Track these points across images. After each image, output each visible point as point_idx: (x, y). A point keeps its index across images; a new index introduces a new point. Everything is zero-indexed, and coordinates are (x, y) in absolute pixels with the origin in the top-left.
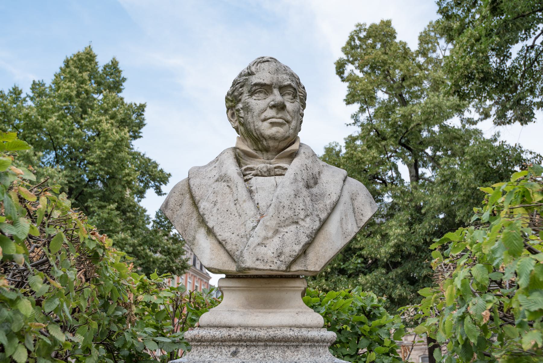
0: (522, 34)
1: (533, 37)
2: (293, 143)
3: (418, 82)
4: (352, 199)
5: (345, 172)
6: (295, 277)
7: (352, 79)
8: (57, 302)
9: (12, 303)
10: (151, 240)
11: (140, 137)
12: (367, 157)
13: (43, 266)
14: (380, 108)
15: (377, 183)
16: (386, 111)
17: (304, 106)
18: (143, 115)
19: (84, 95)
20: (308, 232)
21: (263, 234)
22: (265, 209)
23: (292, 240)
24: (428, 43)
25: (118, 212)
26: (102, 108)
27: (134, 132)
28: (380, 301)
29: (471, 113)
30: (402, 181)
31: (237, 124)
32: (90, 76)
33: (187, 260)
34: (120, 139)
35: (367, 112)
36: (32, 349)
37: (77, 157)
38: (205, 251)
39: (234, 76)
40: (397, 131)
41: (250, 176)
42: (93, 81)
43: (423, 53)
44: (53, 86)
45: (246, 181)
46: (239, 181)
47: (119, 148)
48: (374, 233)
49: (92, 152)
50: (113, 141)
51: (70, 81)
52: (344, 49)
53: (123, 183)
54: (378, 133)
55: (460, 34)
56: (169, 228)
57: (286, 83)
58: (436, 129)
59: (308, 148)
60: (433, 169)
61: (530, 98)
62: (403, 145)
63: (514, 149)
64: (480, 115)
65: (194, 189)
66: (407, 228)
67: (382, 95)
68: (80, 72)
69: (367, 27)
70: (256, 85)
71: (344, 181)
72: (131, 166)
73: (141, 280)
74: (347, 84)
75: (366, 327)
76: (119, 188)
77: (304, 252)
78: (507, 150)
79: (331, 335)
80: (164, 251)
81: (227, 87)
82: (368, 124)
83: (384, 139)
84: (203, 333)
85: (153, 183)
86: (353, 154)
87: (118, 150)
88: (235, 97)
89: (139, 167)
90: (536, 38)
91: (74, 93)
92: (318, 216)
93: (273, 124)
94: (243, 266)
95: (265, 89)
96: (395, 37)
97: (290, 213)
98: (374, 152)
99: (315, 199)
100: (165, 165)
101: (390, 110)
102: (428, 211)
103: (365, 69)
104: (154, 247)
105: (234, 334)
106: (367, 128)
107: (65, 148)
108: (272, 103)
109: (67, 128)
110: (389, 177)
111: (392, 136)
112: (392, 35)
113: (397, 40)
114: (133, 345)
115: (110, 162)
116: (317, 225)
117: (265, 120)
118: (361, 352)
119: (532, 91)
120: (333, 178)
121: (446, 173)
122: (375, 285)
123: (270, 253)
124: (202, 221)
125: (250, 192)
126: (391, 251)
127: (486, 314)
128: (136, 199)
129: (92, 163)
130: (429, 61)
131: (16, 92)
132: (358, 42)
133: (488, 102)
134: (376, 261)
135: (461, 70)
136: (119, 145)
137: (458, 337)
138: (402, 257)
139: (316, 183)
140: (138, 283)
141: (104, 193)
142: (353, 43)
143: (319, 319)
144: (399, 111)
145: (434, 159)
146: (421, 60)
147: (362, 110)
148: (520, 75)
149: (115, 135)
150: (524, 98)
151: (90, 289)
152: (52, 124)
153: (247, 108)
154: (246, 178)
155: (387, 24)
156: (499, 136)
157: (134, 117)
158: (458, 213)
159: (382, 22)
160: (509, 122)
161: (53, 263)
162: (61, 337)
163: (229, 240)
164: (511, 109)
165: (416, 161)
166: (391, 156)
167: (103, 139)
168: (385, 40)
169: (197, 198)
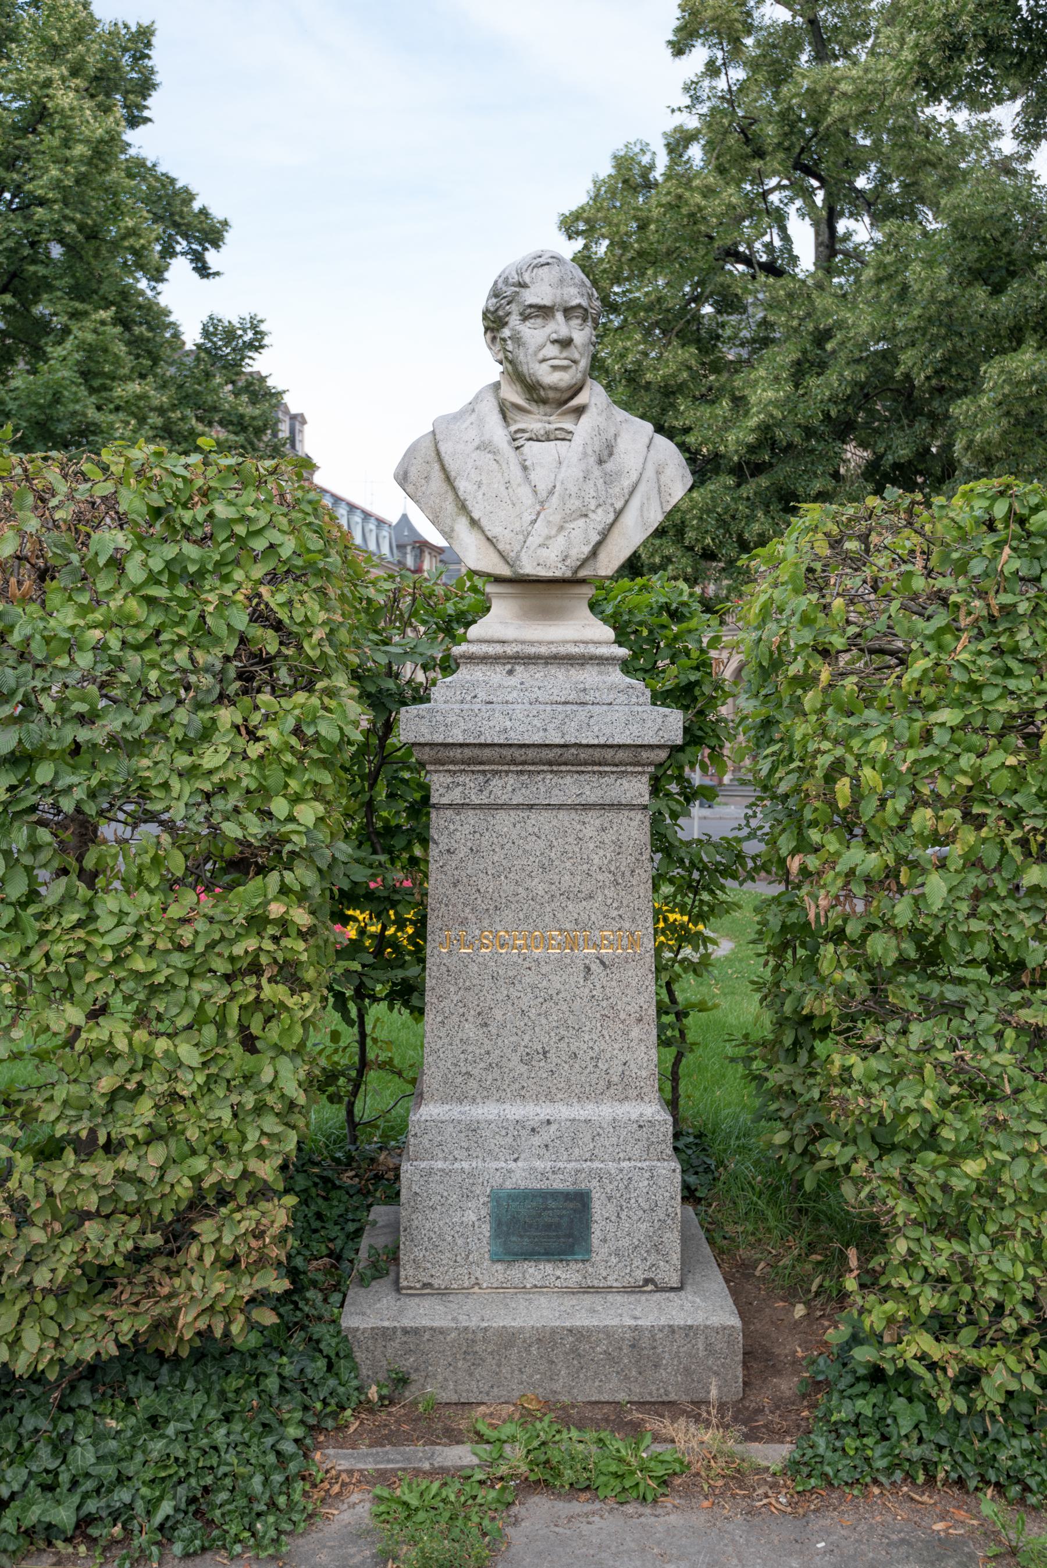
6: (583, 581)
10: (198, 393)
16: (774, 67)
18: (149, 57)
21: (545, 532)
23: (578, 540)
28: (691, 595)
34: (107, 137)
35: (723, 76)
40: (792, 133)
47: (104, 161)
50: (87, 141)
66: (789, 388)
70: (531, 306)
77: (594, 553)
79: (623, 652)
80: (231, 423)
84: (473, 649)
85: (184, 243)
86: (680, 197)
87: (103, 166)
88: (500, 318)
93: (555, 368)
97: (578, 503)
99: (609, 479)
105: (510, 650)
108: (554, 336)
111: (780, 144)
116: (611, 517)
117: (544, 360)
118: (660, 664)
122: (709, 512)
124: (463, 507)
125: (525, 468)
126: (751, 439)
135: (937, 29)
136: (106, 149)
139: (611, 454)
149: (92, 125)
153: (517, 339)
157: (126, 60)
158: (902, 357)
167: (60, 133)
169: (453, 474)
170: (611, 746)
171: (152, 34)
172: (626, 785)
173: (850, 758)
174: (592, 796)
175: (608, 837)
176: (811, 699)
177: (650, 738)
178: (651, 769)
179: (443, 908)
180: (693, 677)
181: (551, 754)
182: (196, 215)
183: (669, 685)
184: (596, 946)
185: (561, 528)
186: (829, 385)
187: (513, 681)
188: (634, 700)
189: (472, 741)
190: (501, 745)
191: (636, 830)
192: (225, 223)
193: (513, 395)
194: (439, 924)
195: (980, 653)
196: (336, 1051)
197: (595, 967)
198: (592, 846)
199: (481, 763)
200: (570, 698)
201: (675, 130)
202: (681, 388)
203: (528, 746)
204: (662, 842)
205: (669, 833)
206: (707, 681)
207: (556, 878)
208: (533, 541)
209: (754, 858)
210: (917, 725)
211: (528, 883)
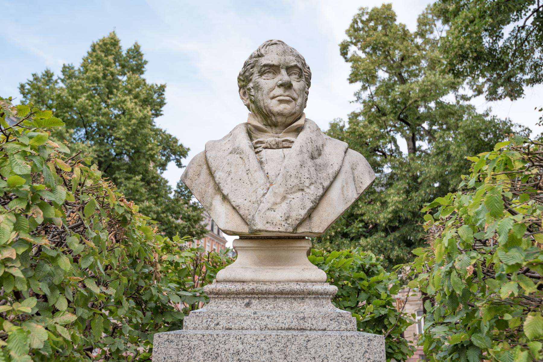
0: (513, 15)
1: (524, 18)
2: (299, 118)
3: (416, 62)
4: (353, 169)
6: (302, 238)
7: (355, 60)
8: (92, 259)
9: (53, 260)
10: (173, 207)
11: (161, 115)
12: (368, 132)
13: (79, 228)
14: (381, 86)
15: (377, 155)
16: (386, 89)
17: (309, 85)
18: (163, 94)
19: (110, 77)
20: (312, 198)
21: (272, 200)
22: (274, 178)
23: (298, 205)
25: (143, 183)
26: (126, 89)
27: (156, 110)
28: (378, 260)
29: (465, 90)
30: (400, 153)
31: (248, 101)
32: (115, 59)
35: (368, 89)
36: (71, 299)
37: (105, 133)
38: (221, 216)
39: (245, 58)
41: (260, 149)
42: (117, 64)
43: (421, 34)
45: (257, 153)
46: (251, 153)
47: (143, 125)
50: (137, 119)
51: (97, 64)
52: (348, 32)
53: (147, 157)
54: (379, 110)
55: (455, 16)
56: (189, 197)
57: (293, 64)
58: (432, 105)
59: (313, 123)
60: (430, 142)
61: (520, 76)
62: (399, 119)
63: (505, 123)
64: (474, 91)
65: (210, 160)
66: (404, 196)
67: (382, 74)
68: (106, 56)
69: (369, 10)
70: (265, 66)
71: (345, 152)
74: (350, 64)
75: (365, 283)
77: (309, 216)
78: (499, 124)
79: (333, 288)
81: (239, 69)
82: (370, 101)
83: (384, 115)
84: (220, 287)
86: (355, 129)
87: (141, 126)
88: (247, 77)
89: (161, 142)
90: (527, 19)
91: (100, 75)
92: (321, 183)
93: (281, 101)
95: (274, 69)
96: (395, 20)
97: (296, 181)
98: (374, 127)
99: (319, 169)
100: (184, 141)
101: (390, 88)
102: (424, 180)
104: (176, 214)
105: (247, 287)
107: (94, 125)
108: (280, 82)
109: (96, 107)
110: (389, 150)
112: (392, 18)
113: (397, 23)
114: (159, 298)
115: (135, 138)
116: (321, 191)
117: (273, 98)
119: (522, 69)
120: (335, 150)
121: (440, 145)
122: (375, 247)
123: (278, 217)
124: (218, 189)
125: (261, 163)
126: (390, 216)
128: (159, 171)
129: (119, 139)
130: (427, 42)
131: (48, 75)
132: (360, 25)
133: (481, 80)
134: (376, 226)
135: (456, 50)
136: (143, 122)
137: (446, 289)
138: (400, 222)
139: (320, 155)
140: (162, 245)
141: (130, 166)
142: (356, 26)
143: (322, 275)
144: (399, 89)
145: (430, 133)
146: (419, 41)
147: (364, 88)
150: (514, 75)
151: (120, 249)
152: (82, 103)
153: (257, 87)
154: (256, 150)
155: (388, 7)
156: (491, 111)
157: (155, 96)
158: (451, 182)
159: (384, 5)
161: (87, 226)
162: (97, 290)
163: (242, 206)
164: (502, 86)
166: (390, 131)
168: (386, 22)
169: (213, 169)
171: (165, 87)
180: (383, 312)
182: (178, 147)
183: (368, 317)
185: (284, 198)
186: (421, 195)
187: (248, 311)
188: (343, 326)
192: (189, 149)
200: (293, 325)
201: (352, 113)
206: (392, 315)
208: (264, 206)
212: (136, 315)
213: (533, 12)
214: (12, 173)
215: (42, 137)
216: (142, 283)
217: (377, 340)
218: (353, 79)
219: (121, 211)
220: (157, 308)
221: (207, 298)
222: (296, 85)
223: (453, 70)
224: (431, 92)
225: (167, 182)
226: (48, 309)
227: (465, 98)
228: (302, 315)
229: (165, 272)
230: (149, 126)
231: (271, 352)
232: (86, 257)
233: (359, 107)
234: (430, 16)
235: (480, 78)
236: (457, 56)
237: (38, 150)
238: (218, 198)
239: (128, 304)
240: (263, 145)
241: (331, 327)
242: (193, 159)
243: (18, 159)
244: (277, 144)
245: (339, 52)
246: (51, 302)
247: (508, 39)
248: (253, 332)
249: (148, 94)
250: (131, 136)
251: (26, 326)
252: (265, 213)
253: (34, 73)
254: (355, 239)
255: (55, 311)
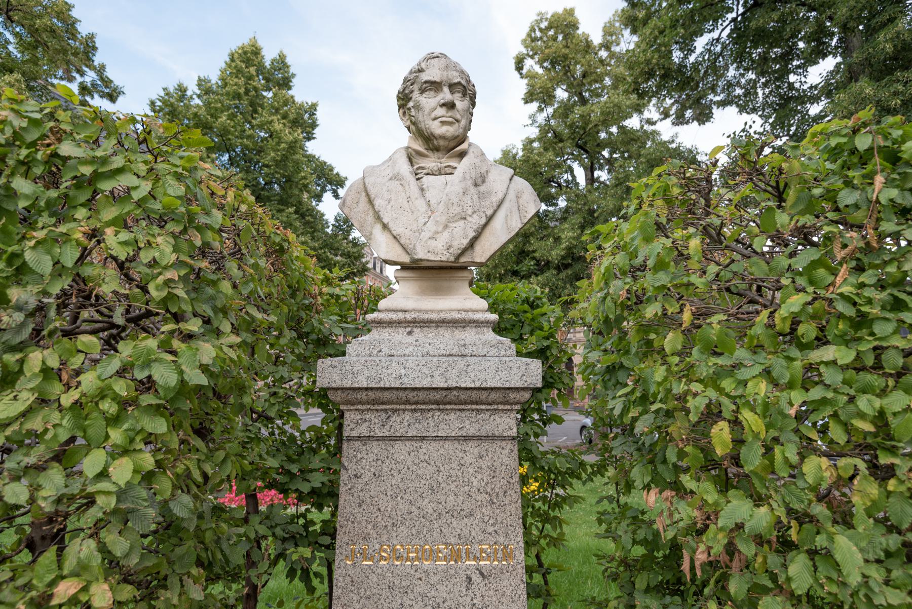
0: (708, 26)
1: (720, 28)
2: (463, 142)
3: (599, 79)
4: (518, 197)
5: (512, 171)
6: (464, 268)
7: (531, 76)
8: (252, 285)
9: (214, 283)
11: (314, 138)
12: (543, 160)
13: (237, 253)
14: (559, 107)
15: (552, 187)
16: (565, 110)
17: (473, 104)
19: (253, 93)
20: (475, 227)
21: (434, 229)
22: (435, 206)
23: (460, 235)
24: (612, 35)
25: (297, 216)
26: (273, 107)
27: (308, 133)
28: (542, 293)
29: (651, 112)
30: (577, 184)
31: (408, 123)
32: (257, 71)
33: (367, 263)
36: (234, 322)
37: (252, 159)
38: (381, 247)
39: (404, 73)
41: (421, 175)
42: (261, 77)
43: (606, 46)
44: (220, 83)
45: (418, 179)
46: (412, 179)
48: (548, 236)
49: (266, 154)
50: (286, 143)
51: (237, 77)
52: (524, 42)
53: (300, 186)
54: (556, 135)
55: (644, 25)
56: (348, 233)
57: (456, 81)
58: (614, 129)
59: (477, 147)
60: (609, 172)
61: (711, 97)
62: (578, 146)
63: (690, 151)
64: (661, 114)
65: (369, 187)
67: (561, 94)
68: (247, 67)
69: (549, 16)
70: (426, 82)
71: (511, 180)
72: (306, 170)
73: (324, 274)
74: (525, 81)
75: (529, 315)
76: (296, 192)
77: (471, 245)
78: (684, 152)
79: (494, 317)
81: (398, 86)
82: (546, 125)
83: (561, 141)
88: (406, 95)
89: (315, 170)
90: (723, 30)
91: (242, 91)
92: (484, 212)
93: (443, 123)
94: (416, 257)
95: (435, 86)
96: (578, 28)
97: (459, 209)
98: (550, 155)
99: (482, 196)
100: (340, 168)
101: (569, 109)
102: (601, 214)
103: (545, 64)
104: (336, 250)
105: (409, 316)
106: (545, 129)
107: (238, 150)
108: (442, 101)
109: (239, 128)
110: (565, 180)
112: (574, 26)
113: (580, 32)
114: (320, 330)
115: (285, 165)
116: (484, 220)
117: (435, 119)
119: (713, 89)
120: (500, 178)
121: (620, 176)
123: (440, 245)
124: (378, 218)
125: (422, 190)
126: (563, 253)
127: (623, 294)
128: (314, 203)
129: (267, 166)
130: (612, 55)
131: (182, 90)
132: (538, 34)
133: (668, 101)
134: (548, 263)
136: (294, 147)
137: (600, 315)
138: (573, 259)
139: (484, 182)
140: (321, 277)
141: (281, 197)
142: (533, 35)
143: (484, 304)
144: (578, 110)
145: (610, 162)
146: (603, 54)
147: (541, 110)
148: (702, 71)
149: (288, 136)
150: (705, 96)
151: (278, 278)
152: (222, 124)
153: (417, 107)
154: (418, 176)
155: (570, 12)
156: (677, 137)
157: (306, 116)
159: (565, 10)
160: (687, 123)
161: (244, 251)
162: (259, 316)
163: (403, 235)
164: (690, 108)
165: (592, 164)
166: (567, 159)
167: (276, 140)
168: (567, 31)
169: (372, 196)
170: (485, 389)
172: (498, 420)
173: (725, 401)
174: (472, 430)
175: (485, 464)
176: (671, 341)
177: (516, 383)
178: (518, 407)
179: (350, 525)
181: (437, 396)
184: (476, 558)
185: (446, 227)
187: (410, 339)
188: (503, 353)
189: (373, 385)
190: (397, 389)
191: (506, 456)
193: (418, 146)
194: (346, 539)
195: (862, 285)
196: (312, 601)
197: (476, 578)
198: (471, 471)
199: (383, 403)
200: (454, 352)
202: (532, 234)
203: (419, 389)
204: (527, 454)
205: (534, 448)
207: (443, 498)
208: (426, 235)
209: (592, 466)
210: (798, 364)
211: (420, 503)
212: (298, 346)
213: (731, 22)
214: (165, 194)
215: (192, 157)
216: (303, 314)
217: (534, 364)
218: (529, 98)
219: (278, 240)
220: (319, 340)
221: (366, 328)
222: (461, 104)
223: (638, 90)
224: (615, 115)
225: (323, 215)
226: (212, 331)
227: (650, 122)
228: (463, 342)
229: (327, 304)
230: (301, 151)
231: (432, 376)
232: (246, 283)
233: (534, 132)
234: (617, 24)
235: (667, 99)
236: (642, 73)
237: (190, 171)
238: (378, 227)
239: (289, 334)
240: (425, 171)
241: (491, 353)
242: (351, 186)
243: (170, 180)
244: (439, 169)
245: (513, 67)
246: (215, 324)
247: (701, 53)
248: (415, 358)
249: (298, 113)
250: (281, 162)
251: (194, 344)
252: (426, 242)
253: (164, 86)
254: (527, 277)
255: (218, 333)
